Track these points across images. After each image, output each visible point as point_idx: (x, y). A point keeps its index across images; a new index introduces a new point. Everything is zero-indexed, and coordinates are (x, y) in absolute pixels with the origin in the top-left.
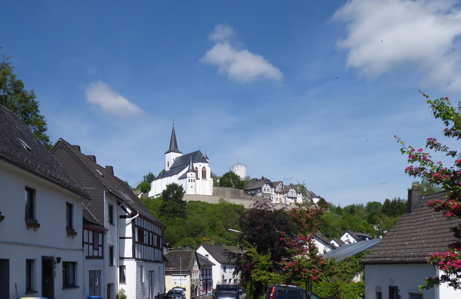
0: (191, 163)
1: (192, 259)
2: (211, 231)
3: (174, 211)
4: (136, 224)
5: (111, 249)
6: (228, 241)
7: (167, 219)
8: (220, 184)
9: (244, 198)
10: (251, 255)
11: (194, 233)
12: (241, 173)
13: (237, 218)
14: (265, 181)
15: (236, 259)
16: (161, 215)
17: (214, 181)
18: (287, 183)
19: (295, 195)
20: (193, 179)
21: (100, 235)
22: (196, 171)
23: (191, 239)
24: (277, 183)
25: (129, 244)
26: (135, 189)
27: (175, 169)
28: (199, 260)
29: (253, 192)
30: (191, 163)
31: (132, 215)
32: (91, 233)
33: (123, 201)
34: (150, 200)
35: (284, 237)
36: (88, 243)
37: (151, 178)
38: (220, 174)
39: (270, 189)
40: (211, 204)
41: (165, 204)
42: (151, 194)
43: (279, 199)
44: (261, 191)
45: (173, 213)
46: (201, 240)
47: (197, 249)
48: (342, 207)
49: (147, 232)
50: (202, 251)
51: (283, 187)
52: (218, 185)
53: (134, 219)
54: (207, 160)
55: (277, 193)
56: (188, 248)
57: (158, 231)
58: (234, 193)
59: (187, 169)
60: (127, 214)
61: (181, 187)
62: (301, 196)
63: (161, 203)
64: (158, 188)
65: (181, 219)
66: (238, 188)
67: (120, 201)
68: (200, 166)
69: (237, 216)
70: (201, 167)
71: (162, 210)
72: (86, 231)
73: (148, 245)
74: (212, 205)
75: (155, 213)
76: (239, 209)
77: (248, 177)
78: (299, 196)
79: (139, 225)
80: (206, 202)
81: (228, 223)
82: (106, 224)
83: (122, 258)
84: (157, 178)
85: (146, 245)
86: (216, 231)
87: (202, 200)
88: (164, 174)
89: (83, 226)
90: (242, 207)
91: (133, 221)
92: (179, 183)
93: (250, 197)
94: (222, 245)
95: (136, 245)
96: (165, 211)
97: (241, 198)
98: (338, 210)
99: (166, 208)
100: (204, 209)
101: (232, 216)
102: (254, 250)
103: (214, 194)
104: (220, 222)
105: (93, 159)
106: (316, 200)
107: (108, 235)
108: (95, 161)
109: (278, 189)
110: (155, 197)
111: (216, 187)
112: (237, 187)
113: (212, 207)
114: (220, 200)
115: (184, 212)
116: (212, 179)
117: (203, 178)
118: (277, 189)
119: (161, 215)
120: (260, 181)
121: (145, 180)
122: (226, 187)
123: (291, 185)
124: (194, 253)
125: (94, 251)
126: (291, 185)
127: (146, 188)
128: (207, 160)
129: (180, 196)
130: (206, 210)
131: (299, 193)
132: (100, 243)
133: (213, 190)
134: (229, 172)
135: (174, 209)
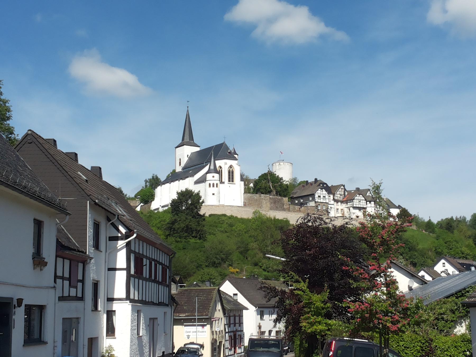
1: (213, 300)
2: (242, 257)
4: (133, 248)
5: (96, 285)
6: (266, 273)
8: (254, 189)
9: (289, 210)
11: (217, 262)
12: (285, 173)
14: (319, 185)
18: (351, 187)
21: (81, 265)
23: (212, 271)
25: (121, 278)
26: (132, 199)
27: (190, 169)
28: (224, 302)
29: (302, 201)
31: (127, 236)
32: (67, 263)
33: (115, 215)
34: (153, 214)
37: (155, 182)
38: (255, 175)
40: (242, 219)
41: (175, 220)
42: (155, 205)
43: (340, 210)
44: (314, 199)
46: (226, 272)
47: (220, 284)
48: (435, 221)
49: (148, 261)
51: (346, 193)
52: (252, 190)
54: (236, 156)
56: (208, 283)
57: (164, 259)
59: (206, 169)
62: (373, 205)
63: (168, 218)
64: (164, 197)
65: (198, 241)
66: (280, 195)
67: (110, 217)
68: (226, 164)
71: (171, 229)
72: (60, 260)
73: (149, 280)
74: (242, 221)
75: (159, 232)
76: (282, 225)
77: (295, 180)
79: (137, 251)
80: (235, 215)
82: (90, 250)
84: (164, 183)
85: (146, 279)
86: (249, 259)
87: (228, 214)
88: (174, 177)
90: (287, 222)
91: (128, 244)
92: (195, 189)
95: (132, 279)
96: (174, 229)
97: (284, 210)
98: (429, 226)
99: (176, 226)
100: (231, 225)
102: (303, 285)
103: (245, 205)
105: (73, 157)
106: (395, 212)
107: (91, 265)
108: (77, 160)
109: (339, 196)
110: (161, 210)
111: (249, 195)
113: (243, 223)
114: (254, 213)
115: (202, 231)
116: (243, 182)
117: (229, 181)
118: (338, 197)
120: (311, 184)
121: (146, 186)
123: (358, 189)
124: (215, 292)
126: (358, 189)
127: (147, 196)
128: (236, 156)
129: (197, 208)
130: (234, 227)
131: (370, 202)
132: (80, 278)
133: (245, 199)
134: (266, 172)
135: (187, 226)
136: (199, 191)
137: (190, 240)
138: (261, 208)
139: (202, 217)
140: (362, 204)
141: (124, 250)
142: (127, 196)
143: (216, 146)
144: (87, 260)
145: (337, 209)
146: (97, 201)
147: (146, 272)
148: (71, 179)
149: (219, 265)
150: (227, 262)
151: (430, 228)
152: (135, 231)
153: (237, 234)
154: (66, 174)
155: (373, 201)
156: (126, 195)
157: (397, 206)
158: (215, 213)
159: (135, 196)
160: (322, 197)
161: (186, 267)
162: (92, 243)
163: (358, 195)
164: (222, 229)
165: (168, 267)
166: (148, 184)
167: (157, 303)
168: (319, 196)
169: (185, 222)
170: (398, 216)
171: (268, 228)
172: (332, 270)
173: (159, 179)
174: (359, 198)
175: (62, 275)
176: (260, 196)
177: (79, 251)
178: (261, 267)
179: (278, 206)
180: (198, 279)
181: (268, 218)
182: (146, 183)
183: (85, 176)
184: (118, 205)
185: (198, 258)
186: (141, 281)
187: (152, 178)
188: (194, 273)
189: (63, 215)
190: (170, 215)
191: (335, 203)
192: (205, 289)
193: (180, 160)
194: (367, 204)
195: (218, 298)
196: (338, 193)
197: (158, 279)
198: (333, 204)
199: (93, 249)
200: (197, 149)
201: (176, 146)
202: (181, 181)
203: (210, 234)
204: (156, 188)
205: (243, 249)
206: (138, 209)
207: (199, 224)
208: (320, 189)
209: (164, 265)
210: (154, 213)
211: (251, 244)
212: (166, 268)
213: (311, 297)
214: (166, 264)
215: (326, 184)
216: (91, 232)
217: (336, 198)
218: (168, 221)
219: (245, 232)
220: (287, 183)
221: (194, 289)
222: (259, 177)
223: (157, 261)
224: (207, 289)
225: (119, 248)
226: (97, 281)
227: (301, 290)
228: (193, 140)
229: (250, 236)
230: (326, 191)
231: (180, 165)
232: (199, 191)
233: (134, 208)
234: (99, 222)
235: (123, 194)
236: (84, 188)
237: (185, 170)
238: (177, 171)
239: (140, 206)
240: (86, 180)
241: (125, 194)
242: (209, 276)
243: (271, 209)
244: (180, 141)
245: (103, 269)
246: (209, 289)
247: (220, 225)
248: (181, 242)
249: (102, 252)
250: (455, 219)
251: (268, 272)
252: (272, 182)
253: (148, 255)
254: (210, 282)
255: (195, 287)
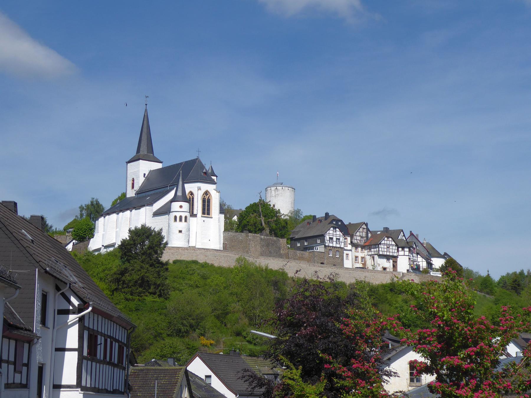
0: (181, 183)
1: (179, 384)
2: (219, 324)
3: (144, 283)
4: (86, 324)
5: (41, 369)
6: (251, 347)
7: (127, 300)
8: (239, 225)
9: (287, 257)
10: (290, 382)
11: (183, 330)
12: (283, 203)
13: (272, 298)
14: (331, 222)
15: (263, 390)
16: (116, 289)
17: (226, 218)
18: (376, 226)
19: (393, 250)
20: (183, 215)
21: (26, 346)
22: (189, 200)
23: (177, 342)
24: (356, 226)
25: (71, 360)
26: (60, 233)
27: (147, 195)
28: (193, 387)
29: (306, 244)
30: (181, 183)
31: (80, 310)
32: (13, 343)
33: (66, 284)
34: (92, 258)
35: (330, 363)
36: (8, 362)
37: (95, 211)
38: (241, 203)
39: (342, 239)
40: (220, 268)
41: (126, 269)
42: (95, 244)
43: (360, 259)
44: (323, 242)
45: (141, 286)
46: (196, 344)
47: (188, 362)
48: (496, 277)
49: (103, 338)
50: (198, 368)
51: (370, 235)
52: (235, 226)
53: (83, 316)
54: (213, 177)
55: (355, 246)
56: (171, 361)
57: (121, 335)
58: (268, 245)
59: (171, 195)
60: (71, 308)
61: (159, 233)
62: (407, 253)
63: (116, 265)
64: (111, 232)
65: (157, 299)
66: (276, 235)
67: (59, 285)
68: (199, 189)
69: (272, 294)
70: (201, 193)
71: (119, 281)
72: (6, 341)
73: (103, 362)
74: (221, 271)
75: (102, 285)
76: (277, 280)
77: (297, 212)
78: (401, 253)
79: (91, 327)
80: (210, 262)
81: (254, 308)
82: (37, 327)
83: (58, 387)
84: (109, 213)
85: (100, 362)
86: (229, 326)
87: (201, 260)
88: (123, 205)
89: (4, 331)
90: (283, 274)
91: (81, 320)
92: (156, 224)
93: (298, 252)
94: (239, 355)
95: (85, 362)
96: (124, 281)
97: (280, 256)
98: (486, 284)
99: (127, 277)
100: (204, 277)
101: (262, 294)
102: (296, 373)
103: (225, 247)
104: (237, 306)
105: (12, 208)
106: (438, 262)
107: (38, 346)
108: (16, 211)
109: (359, 238)
110: (103, 251)
111: (230, 233)
112: (274, 232)
113: (221, 274)
114: (238, 260)
115: (163, 285)
116: (223, 216)
117: (204, 213)
118: (357, 239)
119: (116, 289)
120: (320, 221)
121: (82, 215)
122: (250, 232)
123: (386, 230)
124: (182, 373)
125: (16, 375)
126: (386, 230)
127: (84, 233)
128: (213, 177)
129: (156, 253)
130: (209, 280)
131: (403, 248)
132: (25, 361)
133: (225, 239)
134: (257, 201)
135: (142, 278)
136: (161, 230)
137: (146, 298)
138: (247, 252)
139: (164, 266)
140: (391, 250)
141: (76, 327)
142: (54, 228)
143: (186, 162)
144: (33, 340)
145: (356, 257)
146: (48, 269)
147: (100, 354)
148: (16, 242)
149: (187, 334)
150: (197, 330)
151: (486, 287)
152: (91, 303)
153: (213, 290)
154: (10, 235)
155: (407, 247)
156: (51, 227)
157: (443, 254)
158: (182, 259)
159: (65, 230)
160: (335, 239)
161: (140, 336)
162: (39, 319)
163: (386, 239)
164: (192, 283)
165: (126, 345)
166: (84, 212)
167: (112, 390)
168: (331, 239)
169: (139, 273)
170: (442, 269)
171: (256, 283)
172: (334, 353)
173: (101, 205)
174: (388, 242)
175: (7, 359)
176: (247, 236)
177: (26, 330)
178: (245, 337)
179: (270, 251)
180: (156, 353)
181: (257, 268)
182: (81, 211)
183: (31, 235)
184: (67, 269)
185: (156, 324)
186: (94, 364)
187: (90, 203)
188: (151, 344)
189: (12, 290)
190: (118, 262)
191: (354, 248)
192: (167, 370)
193: (133, 180)
194: (398, 251)
195: (185, 382)
196: (358, 234)
197: (113, 360)
198: (351, 250)
199: (40, 325)
200: (159, 166)
201: (128, 160)
202: (134, 211)
203: (175, 289)
204: (98, 219)
205: (220, 312)
206: (70, 247)
207: (159, 275)
208: (332, 229)
209: (121, 342)
210: (94, 256)
211: (233, 305)
212: (123, 346)
213: (303, 388)
214: (123, 341)
215: (341, 221)
216: (39, 305)
217: (355, 241)
218: (115, 269)
219: (225, 288)
220: (287, 217)
221: (153, 369)
222: (246, 208)
223: (113, 337)
224: (170, 370)
225: (69, 324)
226: (43, 364)
227: (293, 380)
228: (153, 153)
229: (231, 293)
230: (341, 231)
231: (133, 187)
232: (161, 230)
233: (64, 246)
234: (46, 293)
235: (47, 225)
236: (32, 252)
237: (139, 195)
238: (128, 196)
239: (71, 244)
240: (32, 240)
241: (50, 225)
242: (172, 350)
243: (262, 254)
244: (133, 153)
245: (50, 349)
246: (172, 369)
247: (188, 277)
248: (133, 300)
249: (49, 328)
250: (526, 274)
251: (255, 344)
252: (265, 216)
253: (103, 332)
254: (174, 358)
255: (153, 366)
